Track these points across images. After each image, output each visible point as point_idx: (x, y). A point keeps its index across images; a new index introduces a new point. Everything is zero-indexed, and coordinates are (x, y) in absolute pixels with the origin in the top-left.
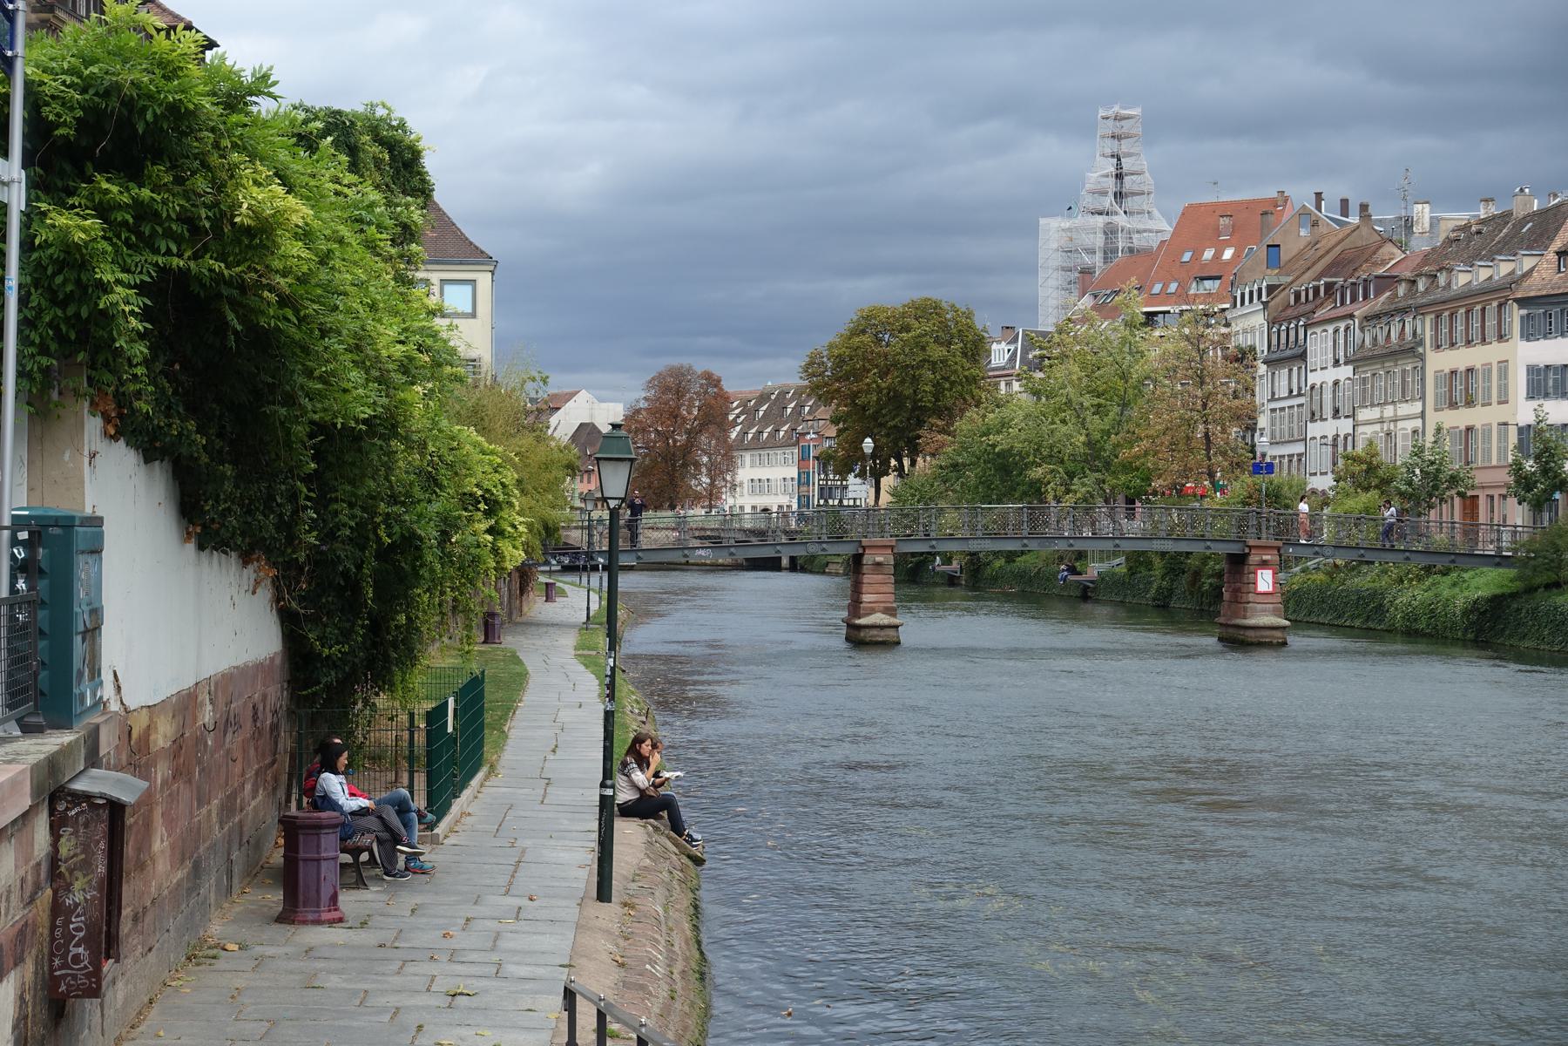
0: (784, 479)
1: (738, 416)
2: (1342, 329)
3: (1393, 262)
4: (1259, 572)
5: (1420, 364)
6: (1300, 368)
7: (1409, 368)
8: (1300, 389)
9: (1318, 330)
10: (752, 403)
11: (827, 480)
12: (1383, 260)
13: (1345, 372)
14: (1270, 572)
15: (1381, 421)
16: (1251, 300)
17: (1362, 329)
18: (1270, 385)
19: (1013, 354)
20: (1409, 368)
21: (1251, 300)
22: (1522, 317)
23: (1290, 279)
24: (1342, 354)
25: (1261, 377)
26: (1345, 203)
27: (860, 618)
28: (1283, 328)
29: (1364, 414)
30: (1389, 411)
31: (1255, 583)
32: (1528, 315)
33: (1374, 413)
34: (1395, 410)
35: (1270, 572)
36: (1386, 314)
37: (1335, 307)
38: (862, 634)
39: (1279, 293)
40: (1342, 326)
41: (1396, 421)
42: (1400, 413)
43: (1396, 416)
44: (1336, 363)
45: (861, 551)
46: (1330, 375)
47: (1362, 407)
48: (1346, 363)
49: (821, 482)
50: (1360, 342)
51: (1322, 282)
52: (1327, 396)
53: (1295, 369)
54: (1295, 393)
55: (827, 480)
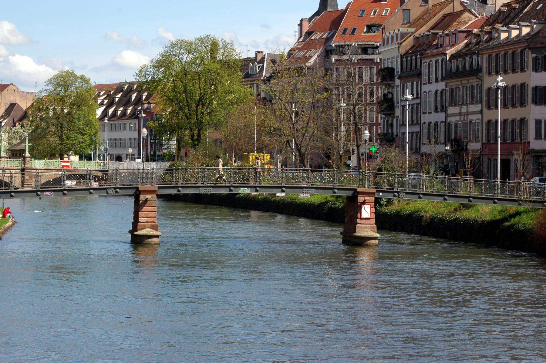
0: (130, 139)
1: (103, 101)
2: (434, 62)
5: (480, 83)
6: (417, 83)
7: (475, 84)
11: (155, 140)
13: (441, 86)
14: (369, 206)
15: (460, 114)
16: (392, 41)
18: (401, 92)
21: (392, 41)
22: (533, 58)
24: (440, 75)
25: (397, 86)
28: (414, 57)
30: (464, 109)
31: (361, 213)
32: (536, 57)
35: (369, 206)
42: (470, 110)
43: (468, 112)
44: (437, 80)
48: (442, 81)
49: (152, 141)
50: (449, 69)
53: (415, 82)
55: (155, 140)
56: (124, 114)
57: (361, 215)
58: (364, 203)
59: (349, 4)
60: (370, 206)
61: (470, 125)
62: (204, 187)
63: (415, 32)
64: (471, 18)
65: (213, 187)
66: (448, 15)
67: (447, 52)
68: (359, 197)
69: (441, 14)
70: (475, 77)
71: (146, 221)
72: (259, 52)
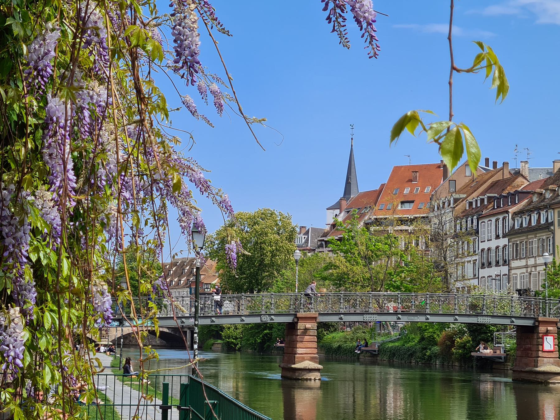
2: (501, 219)
3: (523, 186)
4: (545, 337)
7: (544, 237)
8: (475, 252)
9: (486, 220)
10: (167, 267)
12: (518, 185)
13: (504, 241)
15: (526, 267)
17: (513, 219)
19: (307, 239)
20: (544, 237)
23: (465, 196)
26: (487, 160)
27: (294, 364)
29: (514, 264)
31: (542, 345)
33: (523, 263)
34: (535, 261)
36: (527, 211)
37: (494, 209)
38: (297, 374)
39: (460, 203)
40: (501, 217)
41: (536, 266)
43: (536, 264)
44: (497, 237)
45: (296, 320)
46: (493, 244)
47: (513, 259)
48: (503, 237)
50: (512, 226)
51: (486, 196)
52: (493, 254)
54: (466, 254)
56: (178, 284)
57: (543, 348)
58: (547, 333)
59: (383, 185)
60: (552, 337)
61: (539, 275)
62: (369, 314)
63: (467, 197)
64: (523, 182)
65: (378, 314)
66: (497, 182)
67: (510, 210)
68: (540, 327)
69: (490, 181)
70: (547, 230)
71: (304, 352)
72: (303, 227)
